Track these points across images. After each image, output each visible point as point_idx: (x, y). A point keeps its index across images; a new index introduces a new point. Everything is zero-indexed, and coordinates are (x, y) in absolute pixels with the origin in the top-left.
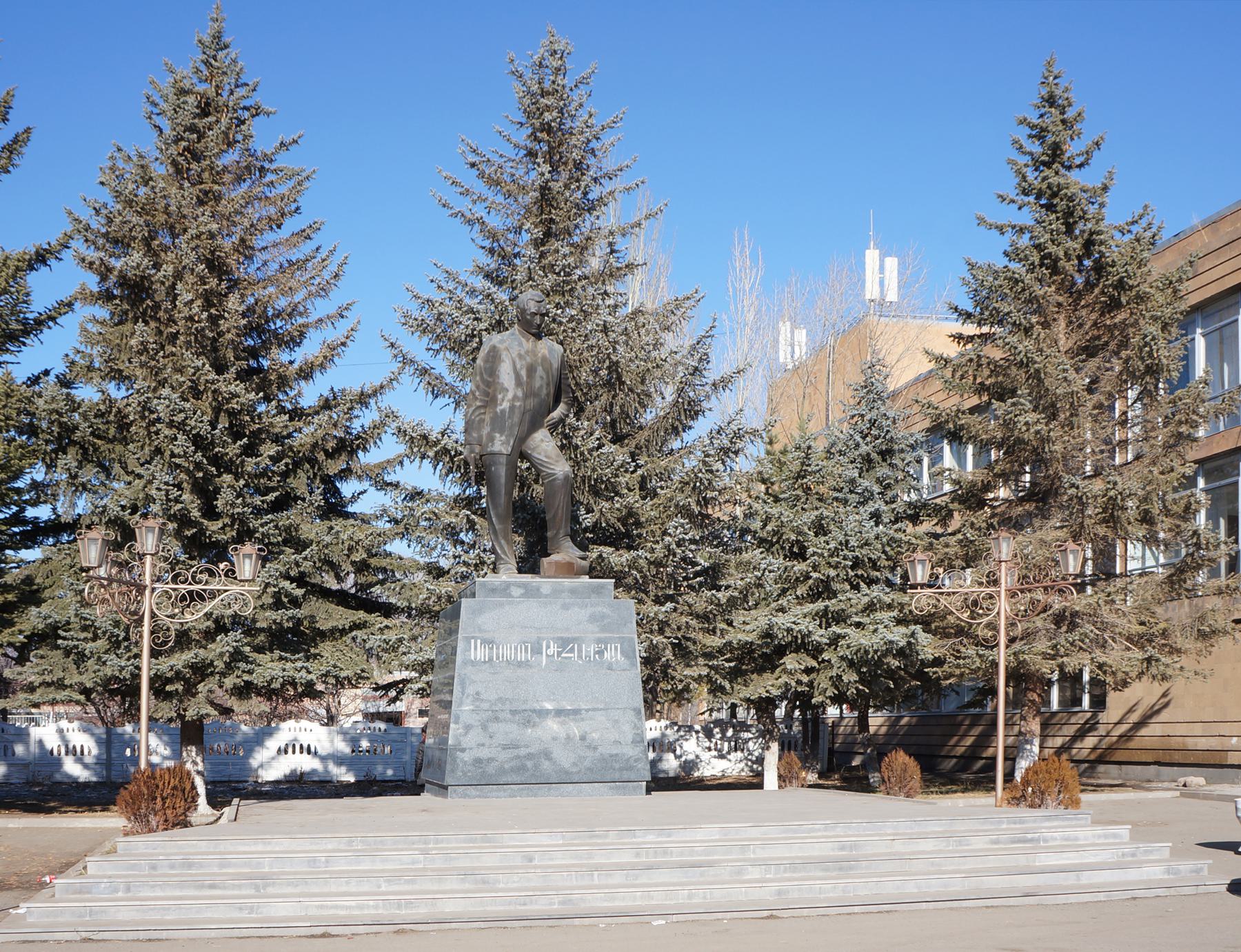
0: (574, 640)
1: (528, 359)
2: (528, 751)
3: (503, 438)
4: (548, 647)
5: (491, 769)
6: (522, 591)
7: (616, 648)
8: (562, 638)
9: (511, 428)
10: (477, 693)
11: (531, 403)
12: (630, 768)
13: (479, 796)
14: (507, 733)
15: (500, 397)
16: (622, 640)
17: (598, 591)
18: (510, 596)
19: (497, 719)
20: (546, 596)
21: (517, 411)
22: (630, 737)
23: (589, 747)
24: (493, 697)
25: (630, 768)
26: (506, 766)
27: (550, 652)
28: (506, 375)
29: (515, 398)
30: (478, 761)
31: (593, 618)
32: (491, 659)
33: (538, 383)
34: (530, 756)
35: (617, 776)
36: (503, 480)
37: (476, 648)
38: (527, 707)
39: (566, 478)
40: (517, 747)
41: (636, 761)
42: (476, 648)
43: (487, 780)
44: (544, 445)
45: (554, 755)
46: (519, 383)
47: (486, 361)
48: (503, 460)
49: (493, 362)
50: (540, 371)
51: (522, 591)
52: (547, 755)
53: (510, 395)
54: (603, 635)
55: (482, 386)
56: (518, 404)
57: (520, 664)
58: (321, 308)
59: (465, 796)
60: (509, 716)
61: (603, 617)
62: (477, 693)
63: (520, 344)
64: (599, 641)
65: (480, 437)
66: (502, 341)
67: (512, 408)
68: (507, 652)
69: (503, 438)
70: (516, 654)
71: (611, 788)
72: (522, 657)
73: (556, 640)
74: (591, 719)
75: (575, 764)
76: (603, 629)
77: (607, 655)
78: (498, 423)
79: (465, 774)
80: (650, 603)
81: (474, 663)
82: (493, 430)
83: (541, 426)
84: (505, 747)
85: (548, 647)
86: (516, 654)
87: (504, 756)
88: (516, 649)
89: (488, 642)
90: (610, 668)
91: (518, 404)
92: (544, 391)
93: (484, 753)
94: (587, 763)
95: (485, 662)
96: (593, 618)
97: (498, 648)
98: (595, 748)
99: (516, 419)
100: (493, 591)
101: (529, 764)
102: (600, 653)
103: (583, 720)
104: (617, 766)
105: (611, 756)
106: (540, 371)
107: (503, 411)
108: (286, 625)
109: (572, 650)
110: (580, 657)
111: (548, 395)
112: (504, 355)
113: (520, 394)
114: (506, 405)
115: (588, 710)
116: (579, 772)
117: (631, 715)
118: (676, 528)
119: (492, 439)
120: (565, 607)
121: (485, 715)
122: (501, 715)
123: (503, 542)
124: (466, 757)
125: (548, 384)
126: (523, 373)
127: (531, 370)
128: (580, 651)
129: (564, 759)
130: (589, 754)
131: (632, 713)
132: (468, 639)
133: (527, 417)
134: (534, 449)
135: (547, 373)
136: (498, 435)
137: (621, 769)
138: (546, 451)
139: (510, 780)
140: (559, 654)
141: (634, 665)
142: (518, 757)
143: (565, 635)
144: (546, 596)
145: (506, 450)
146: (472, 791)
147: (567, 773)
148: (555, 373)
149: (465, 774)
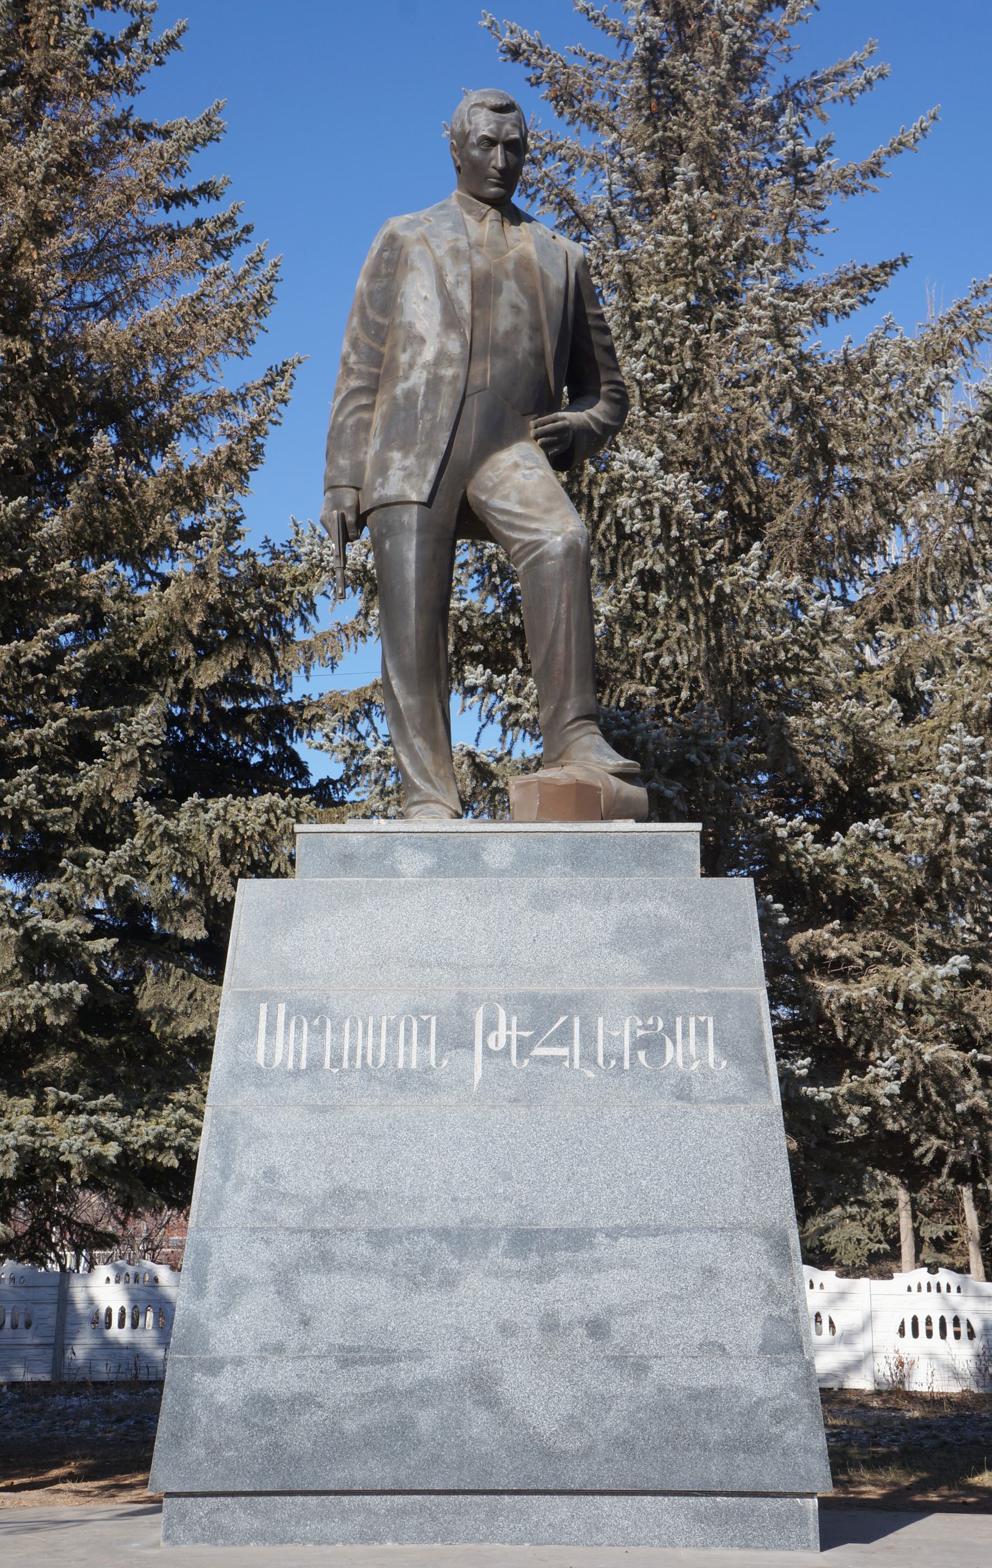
0: (571, 1003)
1: (479, 262)
2: (420, 1371)
3: (411, 461)
4: (491, 1026)
5: (300, 1434)
6: (429, 861)
7: (702, 1031)
8: (533, 999)
9: (430, 435)
10: (270, 1174)
11: (487, 371)
12: (758, 1445)
13: (261, 1537)
14: (354, 1310)
15: (404, 358)
16: (719, 1004)
17: (652, 857)
18: (395, 873)
19: (326, 1262)
20: (501, 873)
21: (446, 390)
22: (752, 1330)
23: (619, 1360)
24: (318, 1186)
25: (758, 1445)
26: (350, 1426)
27: (498, 1040)
28: (420, 306)
29: (442, 357)
30: (263, 1403)
31: (627, 937)
32: (315, 1064)
33: (503, 321)
34: (425, 1392)
35: (714, 1474)
36: (411, 573)
37: (271, 1030)
38: (426, 1219)
39: (571, 550)
40: (387, 1357)
41: (779, 1416)
42: (271, 1030)
43: (280, 1484)
44: (518, 476)
45: (507, 1389)
46: (450, 320)
47: (374, 275)
48: (411, 517)
49: (392, 277)
50: (510, 292)
51: (429, 861)
52: (481, 1386)
53: (428, 354)
54: (656, 989)
55: (364, 340)
56: (448, 372)
57: (403, 1081)
58: (231, 373)
59: (217, 1534)
60: (365, 1250)
61: (660, 930)
62: (270, 1174)
63: (460, 226)
64: (647, 1007)
65: (359, 467)
66: (409, 225)
67: (434, 384)
68: (368, 1044)
69: (411, 461)
70: (392, 1046)
71: (700, 1517)
72: (410, 1056)
73: (513, 1002)
74: (626, 1264)
75: (573, 1424)
76: (662, 969)
77: (673, 1053)
78: (400, 433)
79: (214, 1450)
80: (918, 962)
81: (260, 1076)
82: (387, 445)
83: (520, 435)
84: (349, 1358)
85: (491, 1026)
86: (392, 1046)
87: (342, 1388)
88: (393, 1031)
89: (312, 1013)
90: (683, 1093)
91: (448, 372)
92: (524, 344)
93: (281, 1379)
94: (614, 1421)
95: (297, 1073)
96: (627, 937)
97: (338, 1030)
98: (641, 1368)
99: (445, 411)
100: (347, 861)
101: (426, 1420)
102: (652, 1044)
103: (598, 1265)
104: (715, 1434)
105: (695, 1395)
106: (510, 292)
107: (410, 395)
108: (50, 1017)
109: (563, 1037)
110: (589, 1058)
111: (539, 355)
112: (415, 252)
113: (454, 346)
114: (418, 378)
115: (614, 1234)
116: (587, 1453)
117: (752, 1257)
118: (956, 758)
119: (383, 468)
120: (544, 902)
121: (290, 1247)
122: (342, 1248)
123: (418, 743)
124: (225, 1389)
125: (536, 328)
126: (463, 295)
127: (484, 288)
128: (589, 1038)
129: (540, 1397)
130: (620, 1385)
131: (759, 1245)
132: (248, 1000)
133: (474, 408)
134: (494, 489)
135: (533, 301)
136: (396, 455)
137: (730, 1447)
138: (520, 489)
139: (360, 1475)
140: (524, 1047)
141: (763, 1085)
142: (388, 1394)
143: (546, 988)
144: (501, 873)
145: (418, 491)
146: (237, 1515)
147: (549, 1455)
148: (558, 302)
149: (214, 1450)
